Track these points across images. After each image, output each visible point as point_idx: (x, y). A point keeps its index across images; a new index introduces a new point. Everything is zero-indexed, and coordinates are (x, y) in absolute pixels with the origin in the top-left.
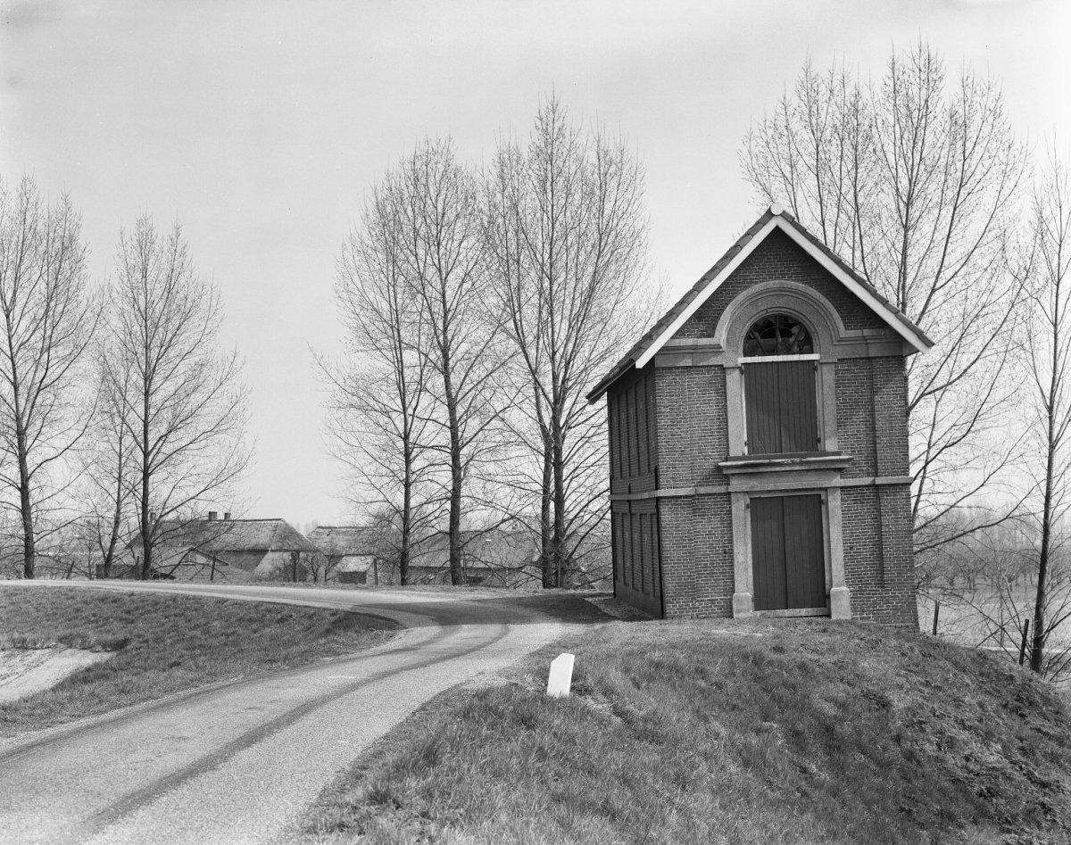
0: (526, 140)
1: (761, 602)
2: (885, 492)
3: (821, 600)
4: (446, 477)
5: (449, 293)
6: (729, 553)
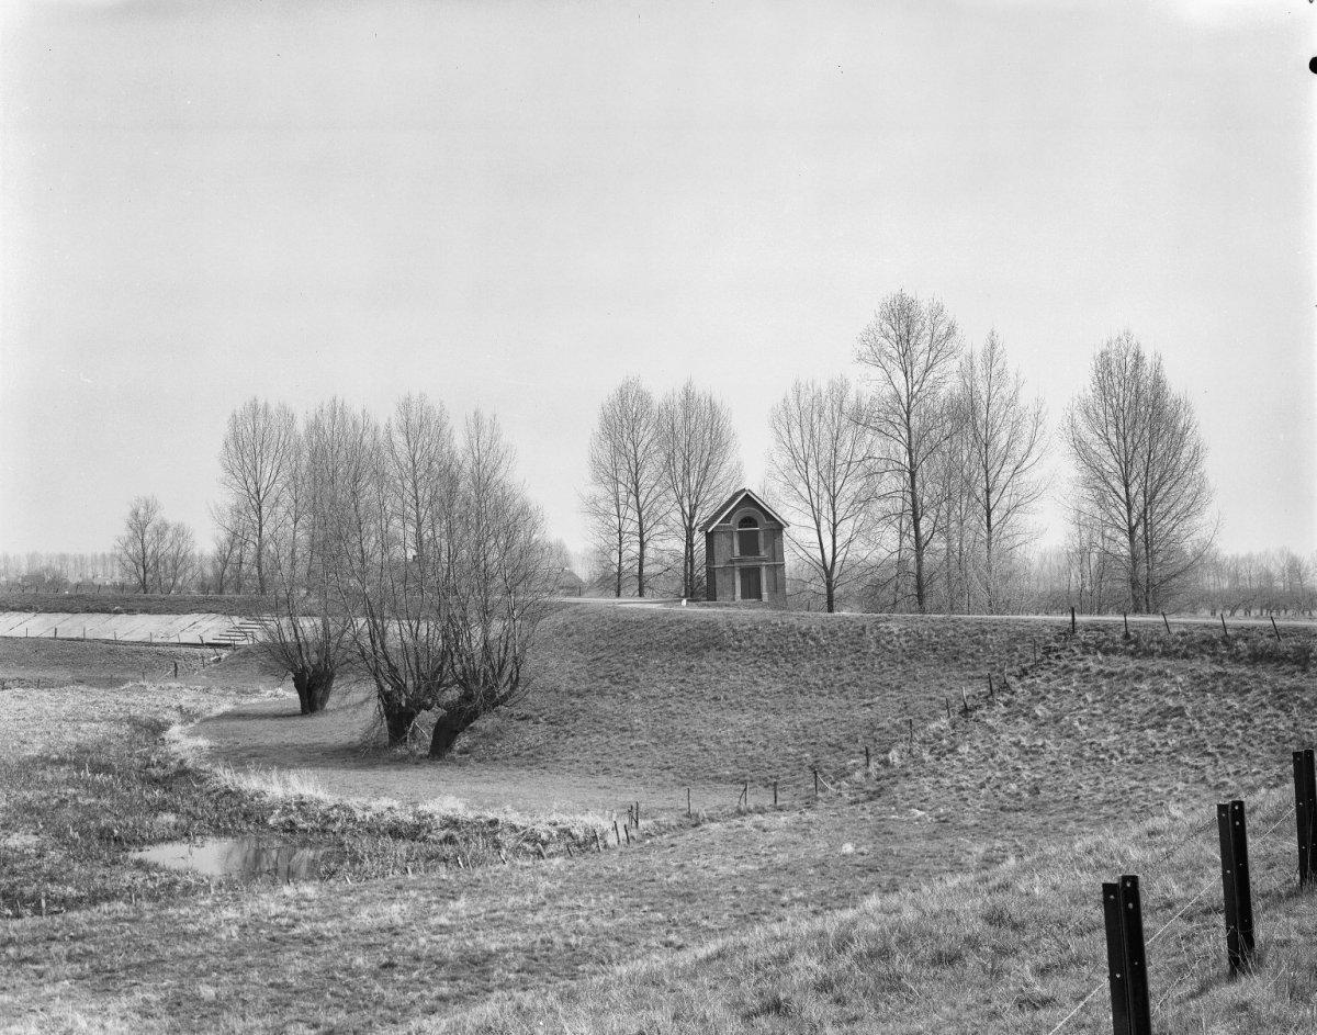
0: (679, 390)
1: (743, 597)
2: (777, 567)
3: (759, 596)
4: (637, 548)
5: (639, 455)
6: (734, 584)
